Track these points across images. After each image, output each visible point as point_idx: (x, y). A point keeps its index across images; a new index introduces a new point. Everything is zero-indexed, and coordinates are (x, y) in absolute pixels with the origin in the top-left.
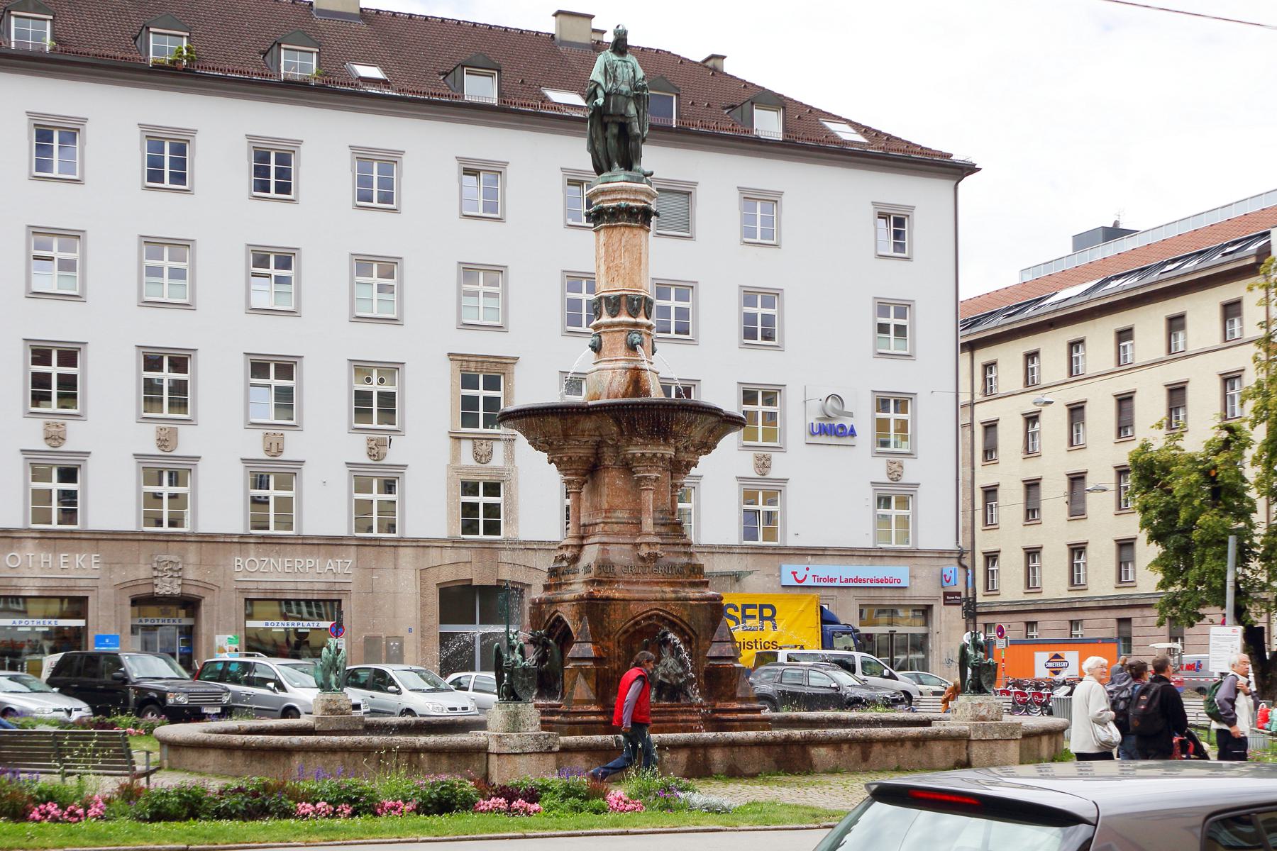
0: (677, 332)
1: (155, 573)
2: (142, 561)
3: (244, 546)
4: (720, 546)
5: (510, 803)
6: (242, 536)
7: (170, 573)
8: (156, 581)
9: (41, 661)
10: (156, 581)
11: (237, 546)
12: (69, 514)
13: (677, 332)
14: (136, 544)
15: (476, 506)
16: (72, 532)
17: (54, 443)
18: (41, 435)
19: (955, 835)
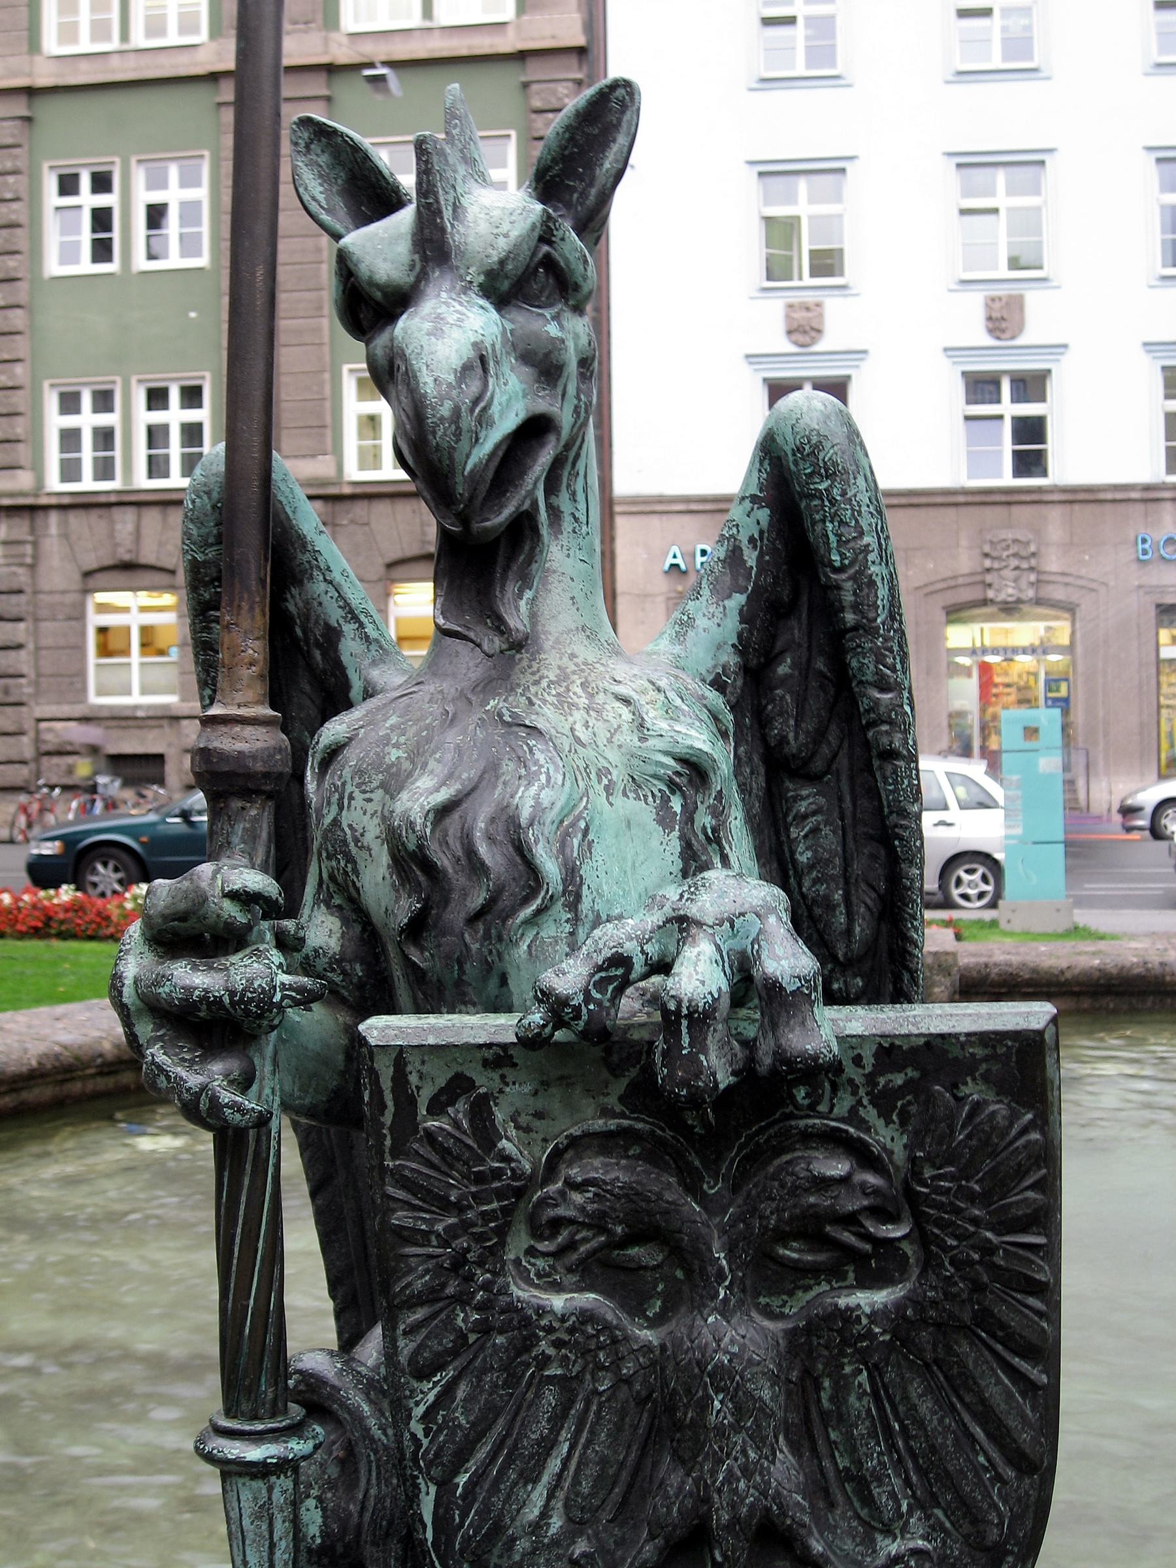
0: (813, 274)
1: (988, 563)
2: (964, 542)
3: (1150, 506)
4: (687, 499)
5: (603, 1368)
6: (1147, 488)
7: (1014, 562)
8: (989, 578)
9: (1008, 827)
10: (989, 578)
11: (1140, 507)
12: (1030, 461)
13: (813, 274)
14: (951, 512)
15: (165, 428)
16: (1040, 490)
17: (801, 338)
18: (780, 327)
19: (295, 1308)
